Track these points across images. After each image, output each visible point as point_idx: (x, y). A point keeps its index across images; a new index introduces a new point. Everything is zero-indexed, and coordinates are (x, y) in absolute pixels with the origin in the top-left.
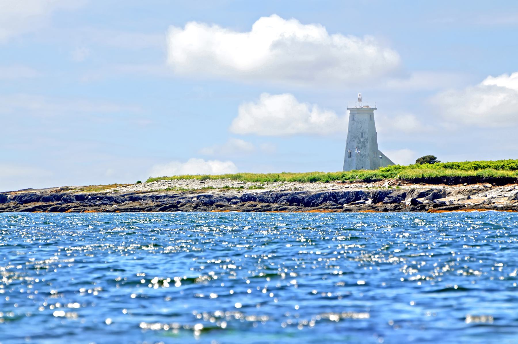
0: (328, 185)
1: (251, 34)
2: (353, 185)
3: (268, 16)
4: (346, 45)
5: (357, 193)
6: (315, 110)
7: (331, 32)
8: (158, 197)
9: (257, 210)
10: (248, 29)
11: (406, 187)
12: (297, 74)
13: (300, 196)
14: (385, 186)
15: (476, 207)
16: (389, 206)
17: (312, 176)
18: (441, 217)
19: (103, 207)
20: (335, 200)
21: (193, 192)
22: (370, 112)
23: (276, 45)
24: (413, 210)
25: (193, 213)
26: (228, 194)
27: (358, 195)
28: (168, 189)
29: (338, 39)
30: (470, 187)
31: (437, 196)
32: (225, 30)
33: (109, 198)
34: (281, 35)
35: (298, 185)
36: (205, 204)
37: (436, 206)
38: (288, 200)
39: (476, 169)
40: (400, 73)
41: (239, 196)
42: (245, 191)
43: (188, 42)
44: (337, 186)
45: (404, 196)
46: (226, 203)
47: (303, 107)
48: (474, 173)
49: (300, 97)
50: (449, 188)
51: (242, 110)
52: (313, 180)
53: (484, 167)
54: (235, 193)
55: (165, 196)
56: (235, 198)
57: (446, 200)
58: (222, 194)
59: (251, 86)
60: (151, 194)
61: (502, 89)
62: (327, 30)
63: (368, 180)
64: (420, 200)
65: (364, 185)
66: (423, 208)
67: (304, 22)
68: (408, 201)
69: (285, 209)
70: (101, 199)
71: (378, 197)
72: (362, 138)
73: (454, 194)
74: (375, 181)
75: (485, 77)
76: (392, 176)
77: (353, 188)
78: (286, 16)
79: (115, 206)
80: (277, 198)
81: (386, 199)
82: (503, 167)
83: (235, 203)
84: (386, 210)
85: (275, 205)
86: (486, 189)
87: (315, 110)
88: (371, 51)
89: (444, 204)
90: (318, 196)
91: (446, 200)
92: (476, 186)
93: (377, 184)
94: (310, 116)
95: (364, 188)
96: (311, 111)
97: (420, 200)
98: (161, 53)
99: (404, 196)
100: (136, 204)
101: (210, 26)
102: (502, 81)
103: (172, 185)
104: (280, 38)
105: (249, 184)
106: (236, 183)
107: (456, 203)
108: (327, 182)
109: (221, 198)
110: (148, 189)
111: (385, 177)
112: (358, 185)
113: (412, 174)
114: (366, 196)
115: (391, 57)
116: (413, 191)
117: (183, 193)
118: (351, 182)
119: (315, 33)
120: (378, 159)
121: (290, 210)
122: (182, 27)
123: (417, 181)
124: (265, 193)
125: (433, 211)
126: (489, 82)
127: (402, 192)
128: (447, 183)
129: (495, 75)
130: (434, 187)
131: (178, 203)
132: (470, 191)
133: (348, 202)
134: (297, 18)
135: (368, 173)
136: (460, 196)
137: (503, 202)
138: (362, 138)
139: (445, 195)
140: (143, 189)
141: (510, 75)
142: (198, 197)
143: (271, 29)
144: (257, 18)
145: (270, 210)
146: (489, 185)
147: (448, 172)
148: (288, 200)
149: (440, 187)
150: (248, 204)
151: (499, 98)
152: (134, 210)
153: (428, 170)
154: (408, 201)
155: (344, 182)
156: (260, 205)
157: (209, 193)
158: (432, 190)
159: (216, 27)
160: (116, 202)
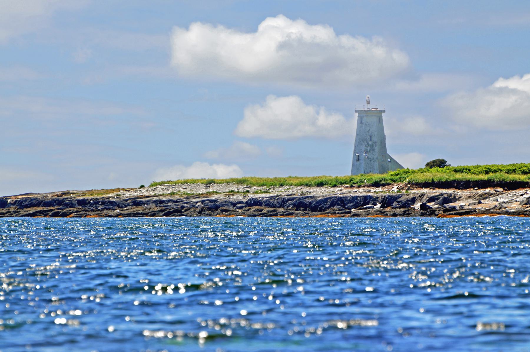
0: (336, 190)
1: (257, 34)
2: (361, 190)
4: (355, 46)
5: (365, 198)
7: (338, 33)
8: (161, 202)
9: (263, 215)
11: (415, 192)
13: (306, 201)
15: (487, 212)
16: (398, 211)
18: (452, 223)
19: (105, 212)
20: (342, 205)
21: (198, 196)
22: (379, 114)
23: (282, 46)
24: (423, 215)
26: (233, 198)
27: (366, 200)
28: (172, 194)
29: (346, 40)
30: (481, 191)
31: (448, 199)
33: (112, 203)
34: (287, 36)
35: (305, 190)
36: (210, 209)
38: (294, 205)
39: (487, 172)
40: (409, 75)
41: (245, 200)
42: (251, 196)
43: (192, 41)
45: (413, 200)
46: (231, 208)
47: (310, 110)
48: (485, 177)
50: (459, 193)
51: (248, 113)
52: (320, 184)
53: (496, 171)
54: (241, 198)
55: (169, 201)
56: (241, 202)
57: (457, 204)
58: (227, 198)
59: (257, 88)
60: (155, 199)
61: (514, 91)
62: (335, 30)
63: (377, 184)
64: (430, 204)
65: (372, 190)
66: (432, 213)
67: (311, 22)
68: (417, 206)
69: (291, 214)
70: (103, 203)
71: (387, 202)
72: (371, 142)
73: (464, 199)
74: (384, 185)
75: (496, 79)
76: (401, 180)
77: (361, 192)
78: (292, 17)
80: (283, 203)
81: (395, 204)
82: (514, 171)
83: (240, 208)
85: (281, 210)
86: (498, 193)
88: (379, 52)
89: (454, 208)
90: (325, 200)
91: (457, 204)
92: (487, 190)
93: (386, 189)
94: (317, 119)
95: (373, 192)
96: (318, 113)
97: (430, 204)
98: (165, 54)
99: (413, 200)
100: (140, 209)
102: (513, 84)
103: (176, 190)
104: (287, 39)
105: (255, 188)
108: (335, 186)
109: (226, 203)
110: (152, 193)
111: (394, 181)
112: (367, 189)
113: (421, 178)
114: (374, 200)
115: (400, 58)
116: (423, 195)
117: (188, 198)
118: (359, 187)
119: (322, 34)
120: (387, 163)
121: (297, 215)
122: (187, 27)
123: (426, 185)
124: (271, 198)
126: (500, 84)
127: (411, 196)
128: (457, 188)
130: (444, 191)
131: (183, 207)
132: (481, 196)
133: (355, 207)
134: (303, 18)
135: (376, 177)
136: (471, 201)
137: (515, 207)
138: (371, 142)
139: (455, 199)
140: (146, 194)
141: (522, 77)
142: (203, 202)
143: (277, 30)
144: (263, 19)
145: (276, 215)
146: (500, 190)
147: (459, 176)
148: (294, 205)
149: (450, 191)
150: (253, 208)
151: (510, 101)
152: (137, 215)
153: (437, 174)
154: (417, 206)
155: (352, 187)
156: (266, 210)
157: (214, 197)
158: (442, 194)
159: (221, 27)
160: (119, 207)
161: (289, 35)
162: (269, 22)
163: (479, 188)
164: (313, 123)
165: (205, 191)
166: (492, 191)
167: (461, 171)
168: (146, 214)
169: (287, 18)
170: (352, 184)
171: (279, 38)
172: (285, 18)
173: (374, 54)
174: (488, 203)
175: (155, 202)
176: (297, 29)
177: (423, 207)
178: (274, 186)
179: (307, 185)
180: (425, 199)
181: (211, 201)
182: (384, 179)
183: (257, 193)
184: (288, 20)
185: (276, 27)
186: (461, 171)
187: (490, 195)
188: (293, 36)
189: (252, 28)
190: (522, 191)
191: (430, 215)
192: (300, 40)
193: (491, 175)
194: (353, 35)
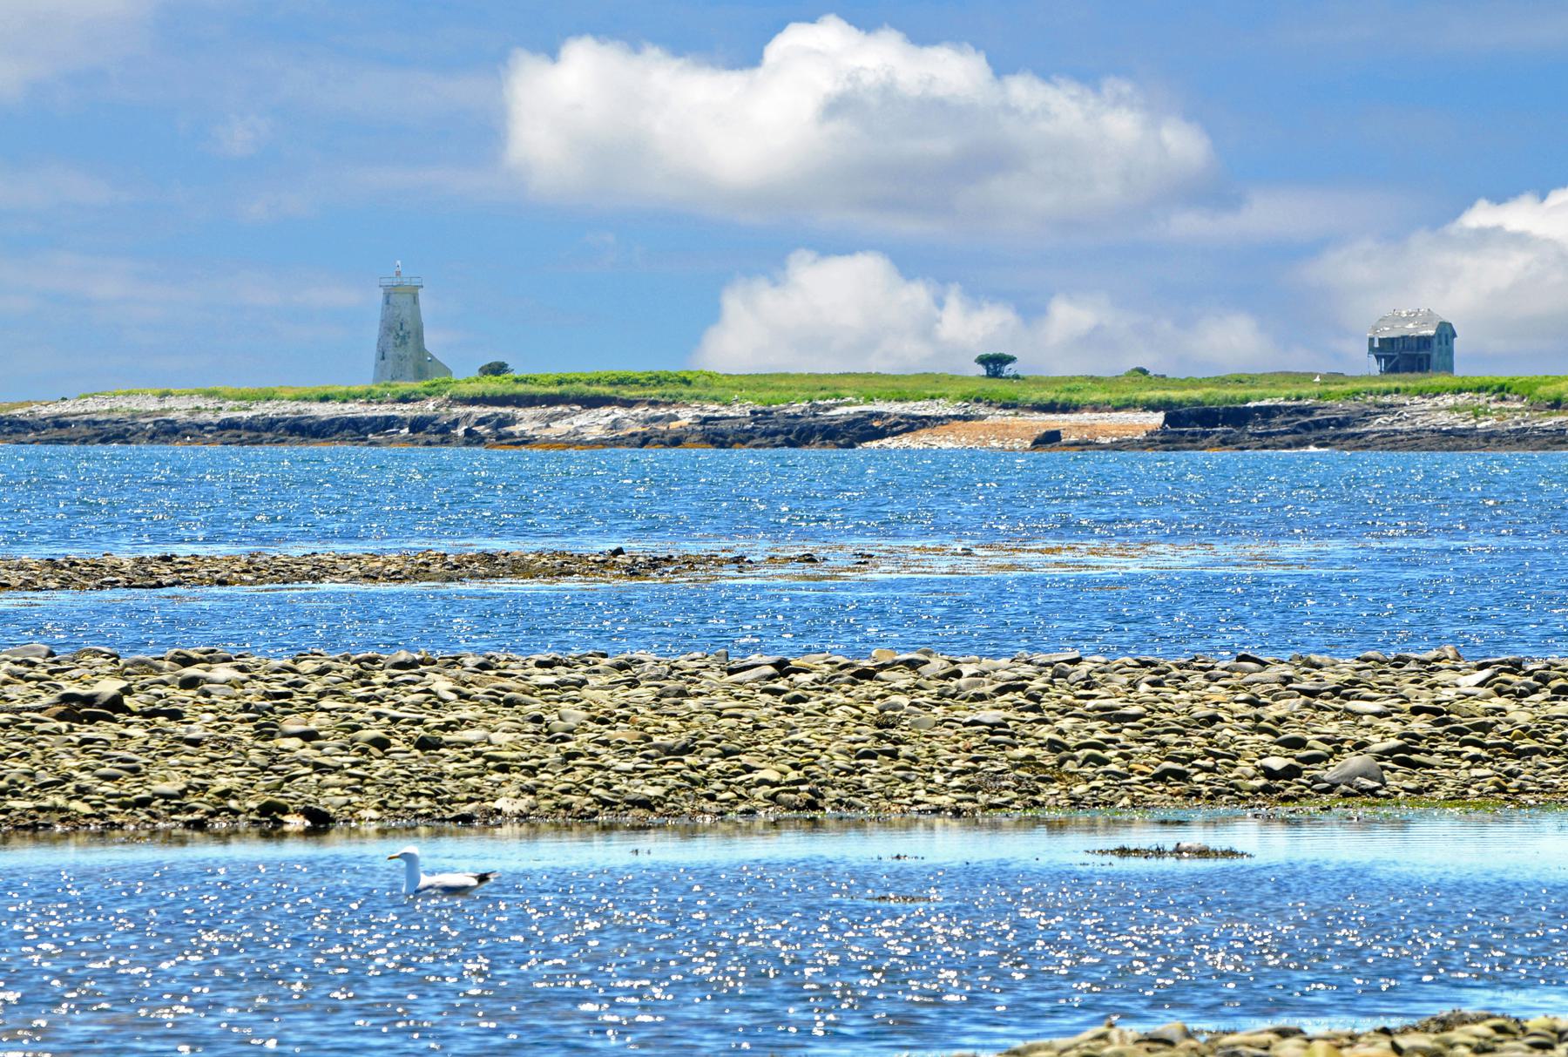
0: (347, 407)
1: (760, 73)
2: (382, 407)
3: (812, 19)
4: (1050, 109)
5: (388, 419)
6: (954, 303)
7: (1001, 68)
8: (95, 423)
9: (242, 443)
10: (747, 55)
11: (459, 410)
12: (900, 196)
13: (304, 423)
14: (429, 407)
16: (433, 438)
17: (323, 392)
18: (500, 455)
19: (14, 436)
20: (355, 429)
21: (148, 414)
23: (835, 107)
24: (467, 444)
25: (150, 447)
27: (388, 423)
28: (111, 411)
29: (1022, 90)
32: (679, 63)
33: (23, 423)
34: (849, 79)
35: (303, 406)
36: (166, 433)
37: (500, 438)
38: (287, 428)
39: (560, 383)
40: (1213, 191)
41: (216, 421)
42: (223, 415)
43: (570, 100)
44: (359, 408)
45: (456, 423)
46: (197, 432)
47: (917, 294)
49: (909, 262)
51: (732, 303)
52: (325, 399)
53: (571, 382)
54: (209, 417)
55: (107, 421)
56: (210, 424)
57: (516, 429)
58: (190, 419)
59: (758, 235)
60: (86, 417)
61: (1521, 240)
62: (990, 61)
63: (404, 399)
64: (478, 429)
65: (399, 407)
66: (481, 441)
67: (920, 36)
68: (460, 431)
69: (283, 441)
70: (11, 423)
71: (418, 425)
72: (402, 340)
73: (527, 421)
74: (414, 401)
75: (1468, 203)
76: (439, 393)
77: (381, 411)
78: (864, 19)
79: (32, 435)
80: (271, 424)
81: (429, 427)
82: (598, 381)
83: (210, 432)
84: (429, 443)
85: (269, 435)
86: (574, 413)
87: (954, 303)
88: (1122, 126)
89: (511, 435)
90: (332, 421)
91: (516, 429)
92: (559, 409)
93: (417, 406)
94: (939, 321)
96: (940, 303)
97: (478, 429)
98: (484, 133)
99: (456, 423)
100: (64, 433)
101: (636, 49)
102: (1519, 216)
103: (117, 404)
104: (849, 86)
105: (230, 403)
106: (211, 403)
107: (529, 433)
108: (345, 401)
109: (191, 425)
110: (80, 409)
111: (429, 395)
112: (390, 406)
113: (468, 390)
115: (1182, 144)
116: (469, 415)
117: (133, 417)
118: (380, 403)
119: (953, 71)
120: (423, 366)
121: (291, 443)
122: (552, 53)
123: (474, 401)
124: (253, 418)
125: (493, 446)
126: (1481, 216)
127: (453, 417)
128: (518, 405)
129: (1501, 196)
130: (499, 410)
131: (127, 430)
132: (550, 416)
133: (375, 431)
134: (897, 26)
135: (405, 387)
136: (536, 424)
137: (595, 433)
138: (402, 340)
139: (513, 421)
140: (73, 410)
141: (1543, 197)
142: (155, 423)
143: (819, 60)
144: (779, 27)
145: (261, 443)
146: (578, 408)
147: (520, 389)
148: (287, 428)
149: (508, 410)
150: (228, 433)
151: (1503, 270)
152: (60, 441)
153: (493, 385)
154: (460, 431)
155: (369, 402)
157: (171, 416)
158: (496, 414)
159: (653, 53)
160: (34, 429)
161: (854, 77)
162: (795, 39)
163: (549, 405)
164: (927, 331)
165: (158, 407)
166: (567, 410)
167: (524, 381)
168: (71, 441)
169: (850, 23)
170: (370, 398)
171: (826, 84)
172: (844, 24)
173: (1107, 133)
174: (560, 428)
175: (86, 422)
176: (879, 58)
177: (468, 432)
178: (257, 399)
179: (305, 399)
180: (472, 420)
181: (167, 422)
182: (415, 392)
183: (233, 410)
184: (853, 30)
185: (817, 52)
186: (524, 381)
187: (562, 415)
188: (868, 79)
189: (745, 54)
190: (607, 410)
191: (478, 444)
192: (887, 91)
193: (565, 387)
194: (1045, 74)
